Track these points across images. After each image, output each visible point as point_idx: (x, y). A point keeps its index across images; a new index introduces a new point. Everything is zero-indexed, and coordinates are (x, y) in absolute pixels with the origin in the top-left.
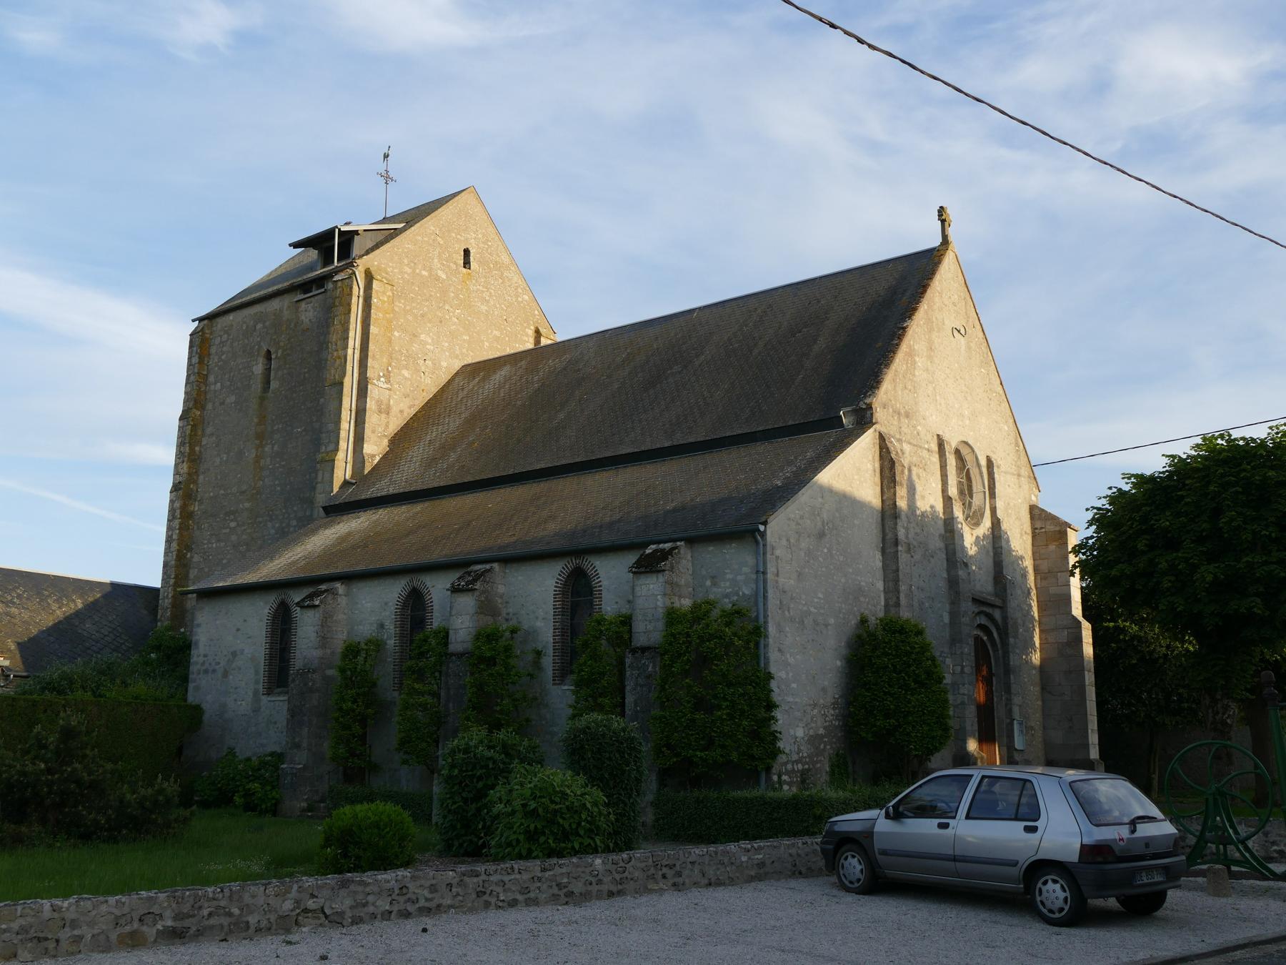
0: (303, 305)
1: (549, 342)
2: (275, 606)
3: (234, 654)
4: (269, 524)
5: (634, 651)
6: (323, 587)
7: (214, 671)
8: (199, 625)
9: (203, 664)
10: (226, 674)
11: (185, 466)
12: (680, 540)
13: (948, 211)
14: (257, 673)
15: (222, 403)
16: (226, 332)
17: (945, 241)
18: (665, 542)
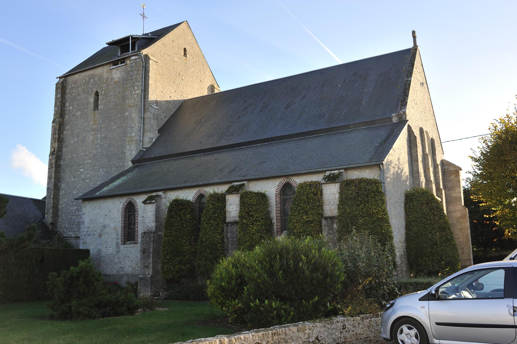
0: (114, 71)
1: (218, 91)
2: (126, 204)
3: (104, 227)
4: (101, 170)
5: (326, 218)
6: (154, 194)
7: (94, 234)
8: (84, 214)
9: (87, 231)
10: (100, 236)
11: (56, 144)
12: (342, 169)
13: (416, 33)
14: (117, 235)
15: (74, 115)
16: (74, 83)
17: (415, 48)
18: (334, 170)
